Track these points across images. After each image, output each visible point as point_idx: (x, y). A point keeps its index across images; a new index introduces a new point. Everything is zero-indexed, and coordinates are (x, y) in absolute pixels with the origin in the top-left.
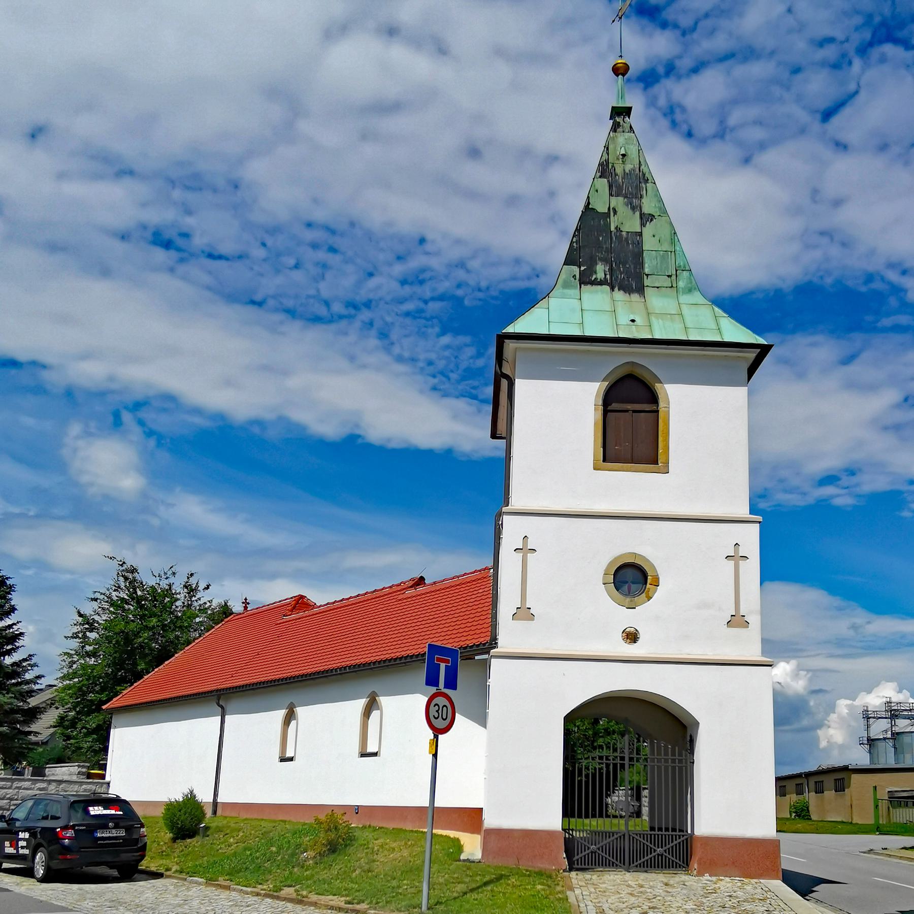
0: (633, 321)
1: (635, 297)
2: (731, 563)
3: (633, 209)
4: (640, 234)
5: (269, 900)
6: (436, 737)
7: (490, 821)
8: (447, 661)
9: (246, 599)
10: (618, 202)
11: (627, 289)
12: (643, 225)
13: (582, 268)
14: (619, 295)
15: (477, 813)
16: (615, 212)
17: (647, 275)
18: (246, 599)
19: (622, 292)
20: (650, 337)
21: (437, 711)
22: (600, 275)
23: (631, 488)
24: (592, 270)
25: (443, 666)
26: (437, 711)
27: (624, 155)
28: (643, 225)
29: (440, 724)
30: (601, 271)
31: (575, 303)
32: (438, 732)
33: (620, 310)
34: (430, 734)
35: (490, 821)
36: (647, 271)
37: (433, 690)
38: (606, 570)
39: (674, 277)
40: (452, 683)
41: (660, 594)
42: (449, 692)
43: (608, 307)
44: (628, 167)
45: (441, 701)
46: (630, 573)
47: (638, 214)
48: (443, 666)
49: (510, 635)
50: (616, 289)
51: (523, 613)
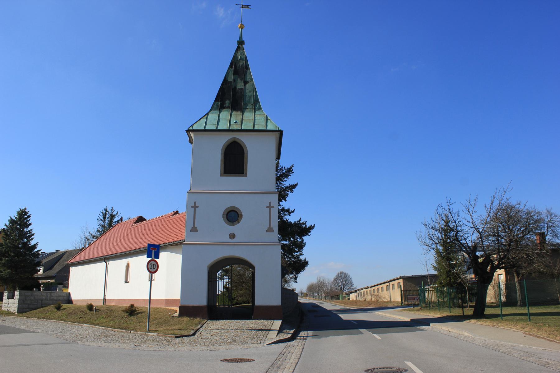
12: (245, 85)
23: (234, 182)
25: (153, 251)
28: (245, 85)
29: (152, 270)
30: (227, 103)
41: (243, 221)
45: (153, 263)
48: (153, 251)
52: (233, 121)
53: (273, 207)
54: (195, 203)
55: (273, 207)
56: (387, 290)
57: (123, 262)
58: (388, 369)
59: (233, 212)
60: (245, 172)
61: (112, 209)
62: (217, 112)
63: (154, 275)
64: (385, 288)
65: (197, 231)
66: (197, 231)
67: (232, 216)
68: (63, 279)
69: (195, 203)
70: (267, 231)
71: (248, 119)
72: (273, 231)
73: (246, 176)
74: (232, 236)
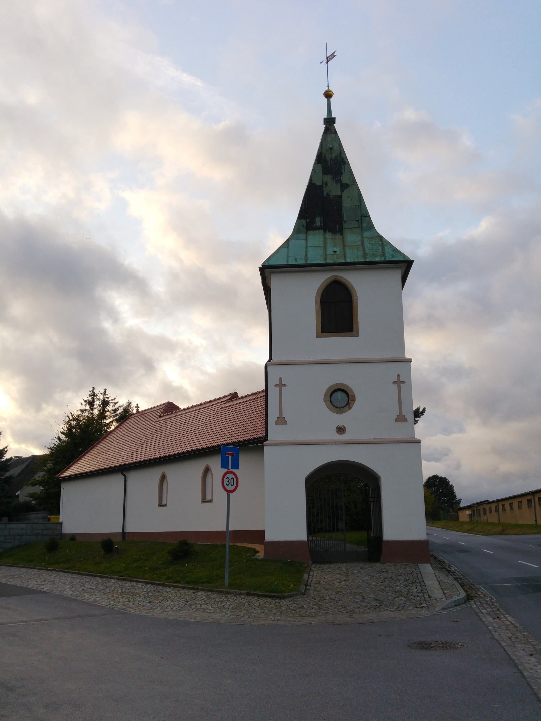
0: (335, 252)
1: (338, 236)
2: (396, 385)
3: (337, 182)
4: (340, 197)
5: (150, 585)
6: (228, 495)
7: (269, 537)
8: (232, 454)
9: (137, 405)
10: (328, 178)
11: (334, 232)
12: (342, 191)
13: (308, 220)
14: (329, 235)
15: (262, 533)
16: (326, 184)
17: (345, 221)
18: (137, 405)
19: (330, 233)
20: (344, 261)
21: (228, 481)
22: (318, 224)
23: (338, 346)
24: (313, 221)
25: (230, 457)
26: (228, 481)
27: (331, 148)
28: (342, 191)
29: (230, 488)
30: (318, 222)
31: (303, 242)
32: (229, 492)
33: (328, 245)
34: (225, 494)
35: (269, 537)
36: (345, 219)
37: (226, 470)
38: (325, 394)
39: (360, 222)
40: (236, 465)
41: (356, 406)
42: (234, 471)
43: (321, 244)
44: (334, 155)
45: (230, 476)
46: (339, 395)
47: (339, 184)
48: (230, 457)
49: (275, 433)
50: (327, 232)
51: (281, 421)
52: (330, 251)
53: (276, 386)
54: (280, 379)
55: (276, 386)
56: (529, 506)
57: (155, 474)
58: (239, 591)
59: (343, 394)
60: (355, 329)
61: (105, 393)
62: (302, 236)
63: (231, 495)
64: (516, 505)
65: (285, 423)
66: (285, 423)
67: (340, 398)
68: (51, 502)
69: (280, 379)
70: (396, 420)
71: (352, 247)
72: (405, 420)
73: (357, 335)
74: (341, 430)
